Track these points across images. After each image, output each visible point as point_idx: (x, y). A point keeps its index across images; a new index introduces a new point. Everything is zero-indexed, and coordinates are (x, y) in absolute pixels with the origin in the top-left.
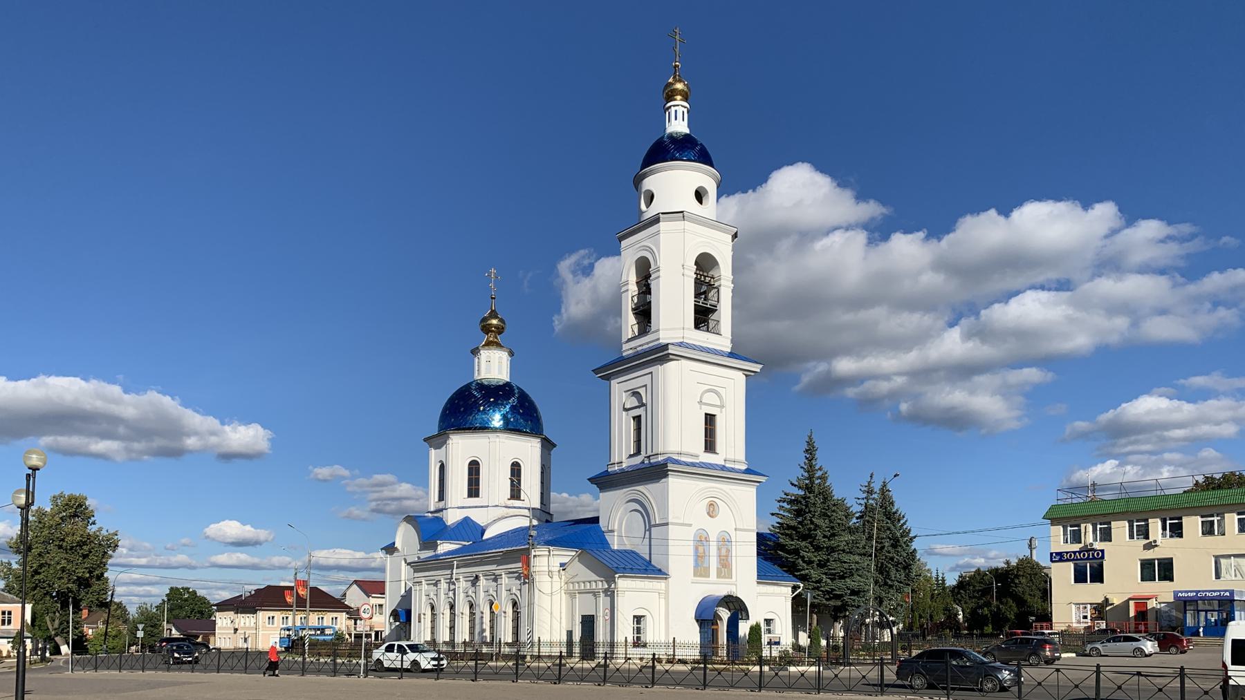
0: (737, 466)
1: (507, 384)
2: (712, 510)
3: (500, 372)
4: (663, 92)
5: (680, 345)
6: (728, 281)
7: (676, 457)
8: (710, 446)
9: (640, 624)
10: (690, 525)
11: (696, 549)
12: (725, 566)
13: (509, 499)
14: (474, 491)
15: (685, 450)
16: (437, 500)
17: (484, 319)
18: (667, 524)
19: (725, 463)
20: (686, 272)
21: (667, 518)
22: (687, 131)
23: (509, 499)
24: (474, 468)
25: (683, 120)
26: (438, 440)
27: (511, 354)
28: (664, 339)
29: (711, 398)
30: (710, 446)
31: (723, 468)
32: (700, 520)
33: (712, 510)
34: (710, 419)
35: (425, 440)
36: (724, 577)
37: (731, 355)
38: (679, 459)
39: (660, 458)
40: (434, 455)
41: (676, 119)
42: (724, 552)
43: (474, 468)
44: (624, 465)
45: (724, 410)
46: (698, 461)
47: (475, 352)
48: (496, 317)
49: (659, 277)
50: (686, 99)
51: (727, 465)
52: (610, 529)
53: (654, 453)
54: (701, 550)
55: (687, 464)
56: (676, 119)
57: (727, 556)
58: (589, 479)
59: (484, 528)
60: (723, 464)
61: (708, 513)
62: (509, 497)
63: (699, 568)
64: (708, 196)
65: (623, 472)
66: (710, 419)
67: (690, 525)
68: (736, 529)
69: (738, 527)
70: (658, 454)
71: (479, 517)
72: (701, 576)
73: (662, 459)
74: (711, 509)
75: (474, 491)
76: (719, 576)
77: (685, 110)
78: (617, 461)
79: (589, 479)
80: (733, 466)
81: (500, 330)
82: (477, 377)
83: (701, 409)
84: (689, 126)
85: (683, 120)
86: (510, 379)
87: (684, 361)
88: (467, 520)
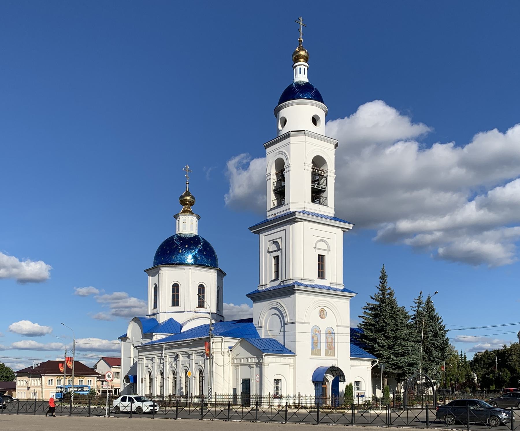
0: (338, 287)
1: (196, 237)
2: (322, 314)
3: (192, 229)
4: (292, 57)
5: (303, 212)
6: (332, 173)
7: (300, 281)
8: (321, 274)
9: (278, 384)
10: (309, 323)
11: (313, 338)
12: (331, 349)
13: (197, 307)
14: (175, 302)
15: (306, 277)
16: (153, 307)
17: (182, 197)
18: (295, 323)
19: (331, 285)
20: (307, 167)
21: (295, 319)
22: (307, 81)
23: (197, 307)
24: (176, 288)
25: (305, 74)
26: (153, 271)
27: (199, 218)
28: (293, 209)
29: (322, 245)
30: (321, 274)
31: (329, 288)
32: (315, 320)
33: (322, 314)
34: (321, 258)
35: (146, 271)
36: (330, 355)
37: (335, 218)
38: (302, 282)
39: (290, 282)
40: (151, 281)
41: (300, 73)
42: (330, 340)
43: (176, 288)
44: (268, 287)
45: (330, 252)
46: (314, 284)
47: (176, 217)
48: (189, 195)
49: (290, 170)
50: (306, 61)
51: (332, 286)
52: (259, 326)
53: (287, 278)
54: (315, 338)
55: (307, 286)
56: (300, 73)
57: (332, 342)
58: (246, 295)
59: (182, 325)
60: (329, 286)
61: (320, 316)
62: (197, 306)
63: (315, 350)
64: (320, 120)
65: (267, 291)
66: (321, 258)
67: (309, 323)
68: (337, 326)
69: (338, 324)
70: (289, 280)
71: (179, 319)
72: (316, 354)
73: (292, 282)
74: (322, 313)
75: (175, 302)
76: (327, 355)
77: (306, 68)
78: (264, 284)
79: (246, 295)
80: (335, 287)
81: (192, 203)
82: (177, 232)
83: (315, 251)
84: (308, 78)
85: (305, 74)
86: (198, 234)
87: (305, 223)
88: (171, 320)
